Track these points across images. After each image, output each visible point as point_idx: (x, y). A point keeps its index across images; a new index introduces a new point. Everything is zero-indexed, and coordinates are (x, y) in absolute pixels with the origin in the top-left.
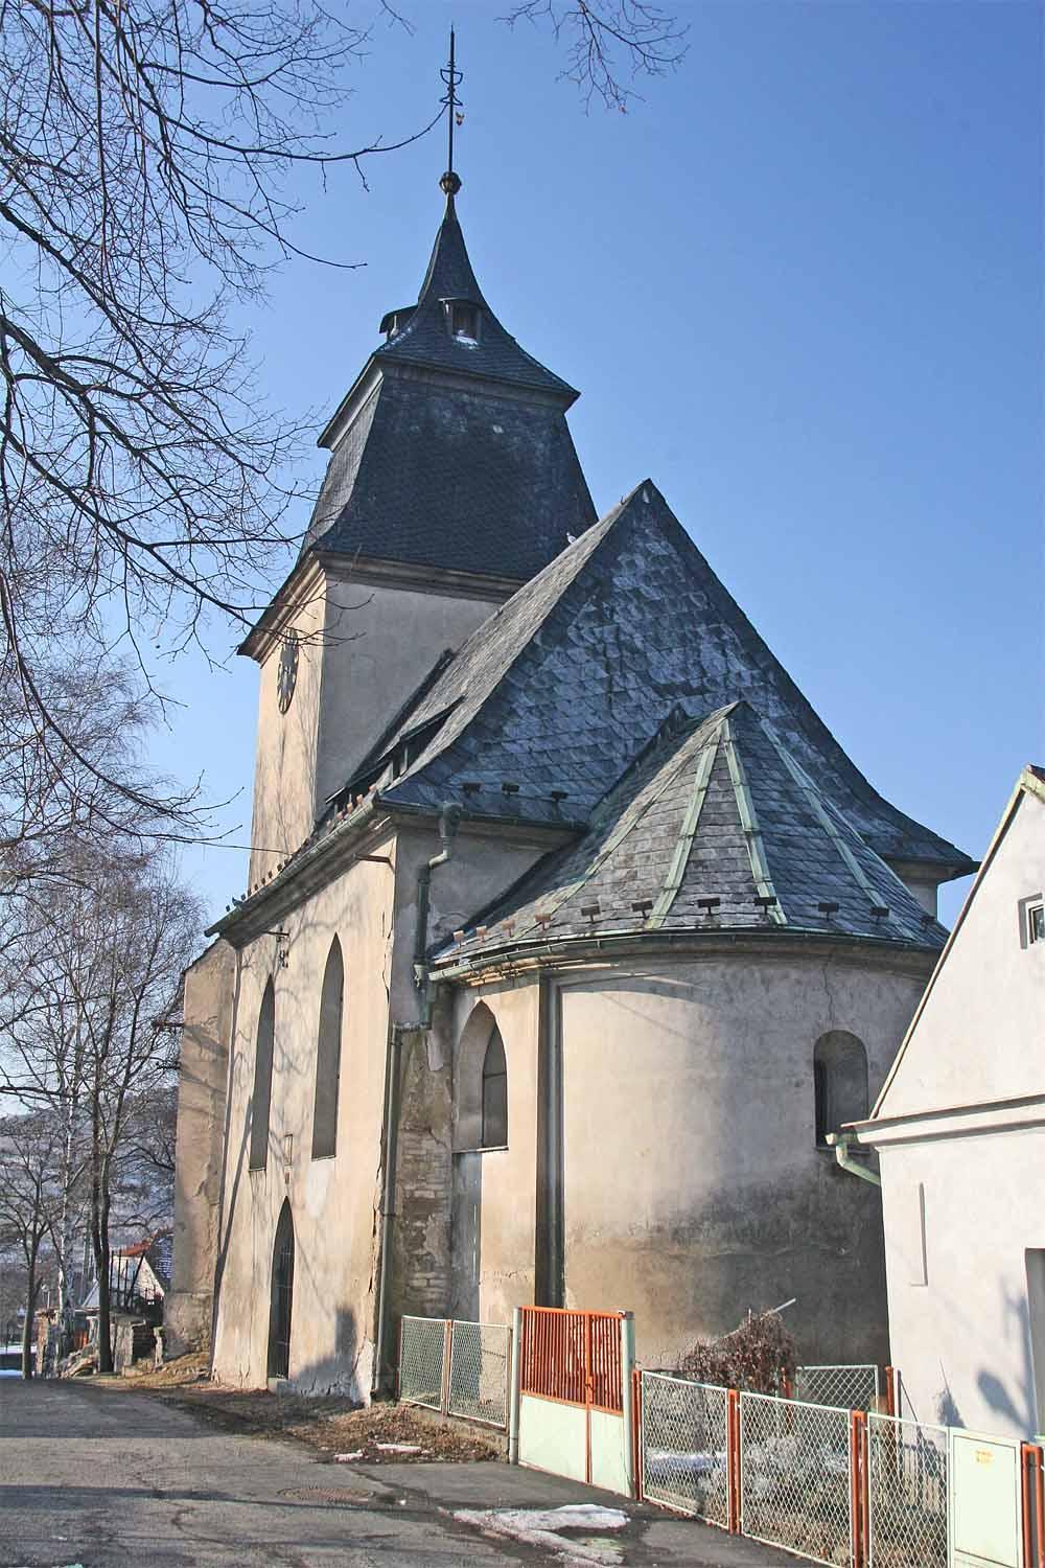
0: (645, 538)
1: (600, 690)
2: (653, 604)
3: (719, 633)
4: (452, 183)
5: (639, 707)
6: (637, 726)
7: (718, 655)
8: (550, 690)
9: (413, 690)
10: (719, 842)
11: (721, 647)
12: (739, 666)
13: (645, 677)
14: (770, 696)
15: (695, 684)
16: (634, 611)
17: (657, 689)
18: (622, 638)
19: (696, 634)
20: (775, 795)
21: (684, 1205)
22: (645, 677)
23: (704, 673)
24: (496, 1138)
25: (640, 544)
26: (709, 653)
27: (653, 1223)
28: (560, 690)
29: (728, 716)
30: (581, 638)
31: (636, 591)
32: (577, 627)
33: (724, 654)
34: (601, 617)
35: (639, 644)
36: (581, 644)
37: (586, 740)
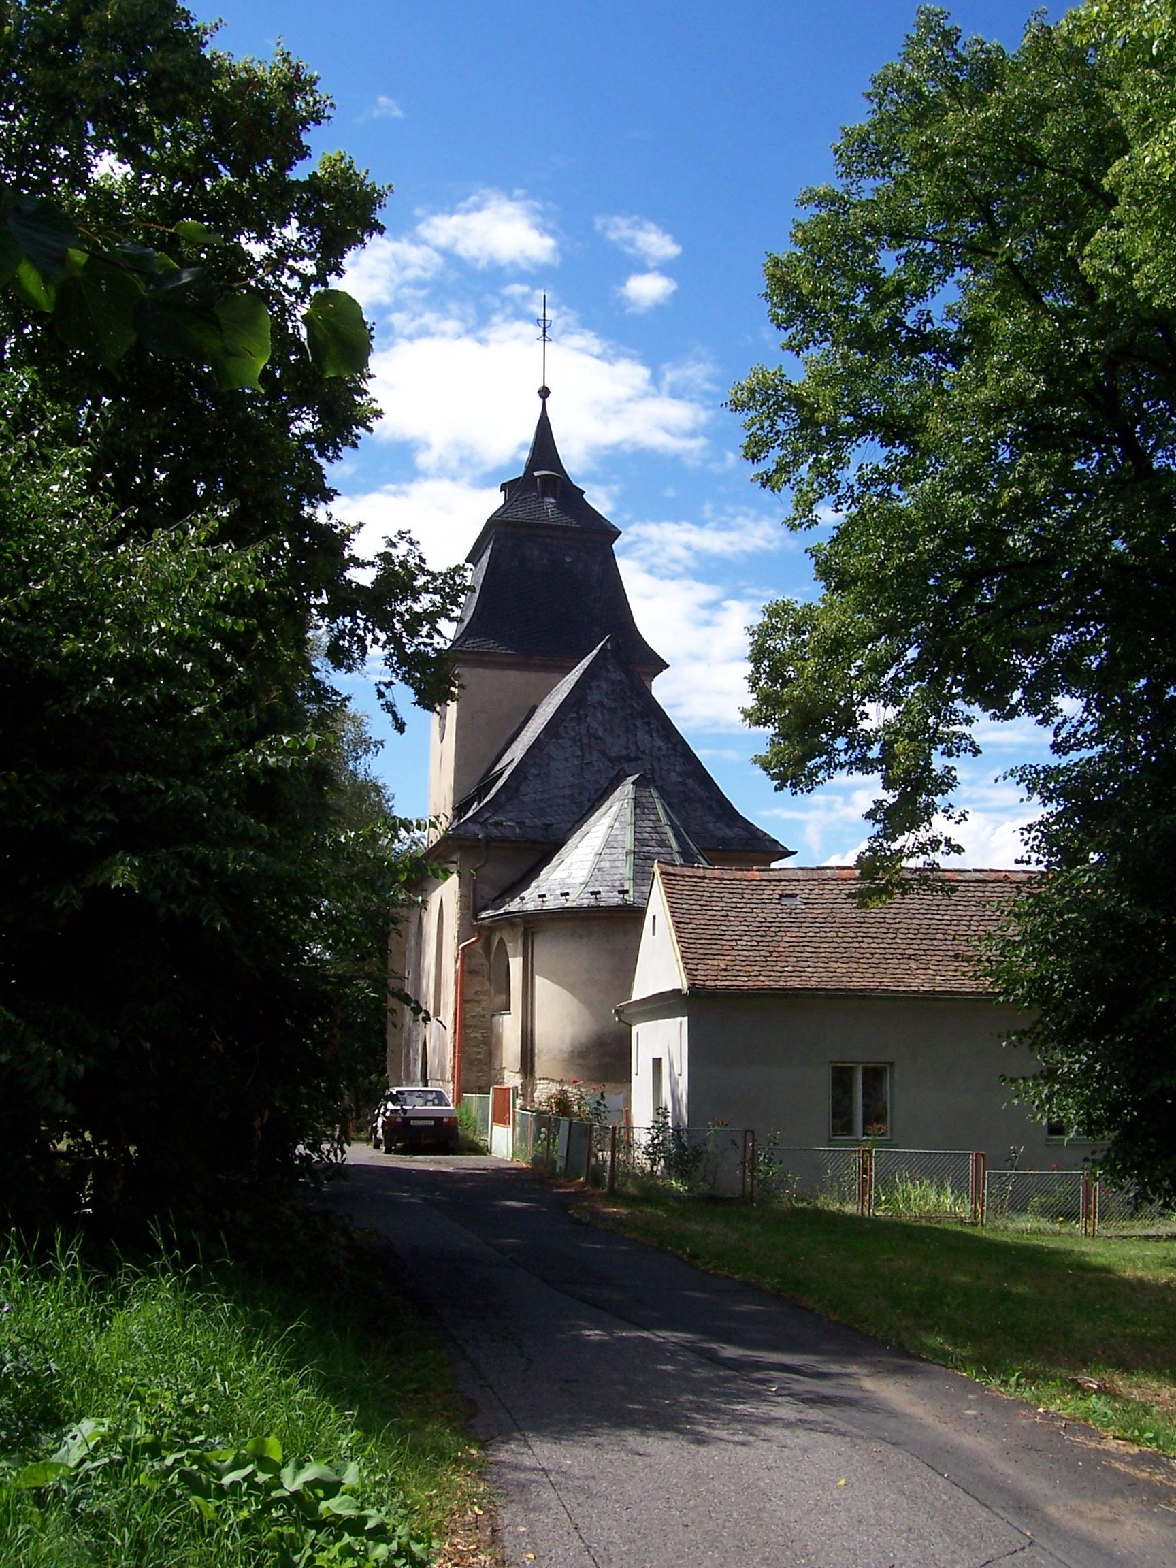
0: (608, 671)
1: (577, 762)
2: (610, 710)
3: (648, 724)
4: (544, 393)
5: (599, 771)
6: (597, 782)
7: (647, 738)
8: (548, 765)
9: (515, 728)
10: (611, 857)
11: (650, 732)
12: (659, 743)
13: (603, 753)
14: (678, 759)
15: (632, 755)
16: (599, 715)
17: (611, 760)
18: (591, 731)
19: (635, 726)
20: (648, 829)
21: (583, 1040)
22: (603, 753)
23: (638, 748)
24: (507, 1008)
25: (604, 674)
26: (642, 736)
27: (570, 1049)
28: (553, 764)
29: (633, 783)
30: (567, 732)
31: (601, 703)
32: (565, 727)
33: (651, 737)
34: (579, 720)
35: (600, 734)
36: (567, 736)
37: (567, 792)
